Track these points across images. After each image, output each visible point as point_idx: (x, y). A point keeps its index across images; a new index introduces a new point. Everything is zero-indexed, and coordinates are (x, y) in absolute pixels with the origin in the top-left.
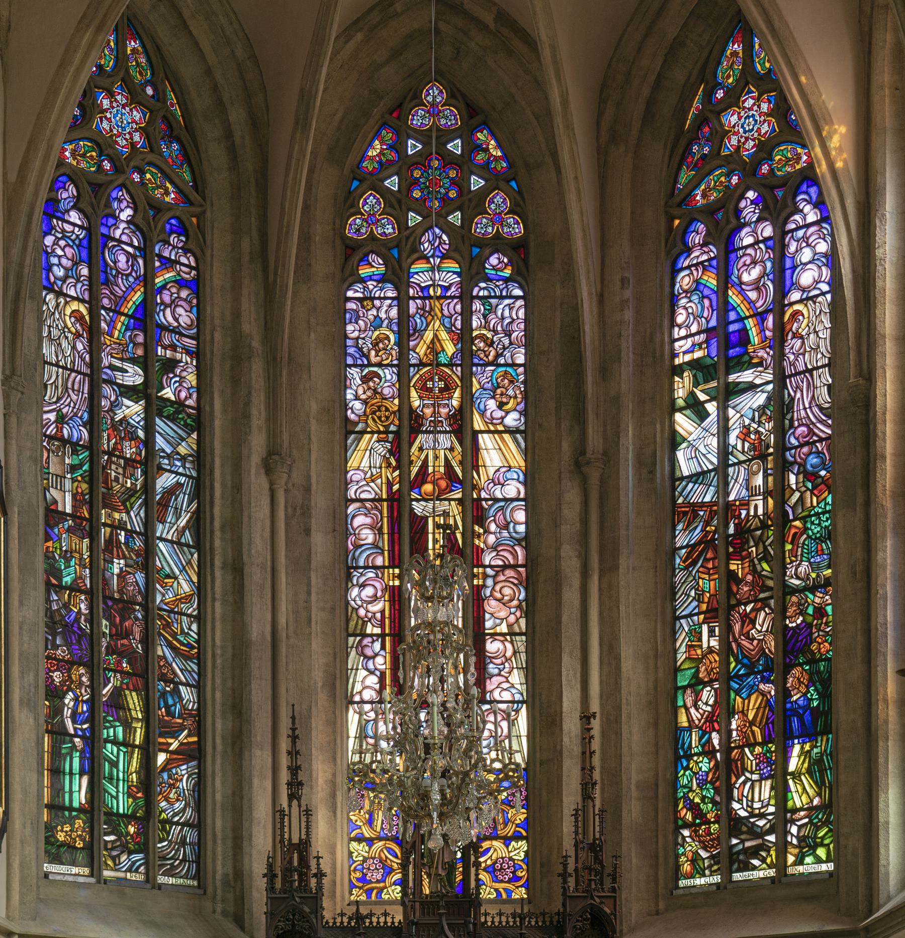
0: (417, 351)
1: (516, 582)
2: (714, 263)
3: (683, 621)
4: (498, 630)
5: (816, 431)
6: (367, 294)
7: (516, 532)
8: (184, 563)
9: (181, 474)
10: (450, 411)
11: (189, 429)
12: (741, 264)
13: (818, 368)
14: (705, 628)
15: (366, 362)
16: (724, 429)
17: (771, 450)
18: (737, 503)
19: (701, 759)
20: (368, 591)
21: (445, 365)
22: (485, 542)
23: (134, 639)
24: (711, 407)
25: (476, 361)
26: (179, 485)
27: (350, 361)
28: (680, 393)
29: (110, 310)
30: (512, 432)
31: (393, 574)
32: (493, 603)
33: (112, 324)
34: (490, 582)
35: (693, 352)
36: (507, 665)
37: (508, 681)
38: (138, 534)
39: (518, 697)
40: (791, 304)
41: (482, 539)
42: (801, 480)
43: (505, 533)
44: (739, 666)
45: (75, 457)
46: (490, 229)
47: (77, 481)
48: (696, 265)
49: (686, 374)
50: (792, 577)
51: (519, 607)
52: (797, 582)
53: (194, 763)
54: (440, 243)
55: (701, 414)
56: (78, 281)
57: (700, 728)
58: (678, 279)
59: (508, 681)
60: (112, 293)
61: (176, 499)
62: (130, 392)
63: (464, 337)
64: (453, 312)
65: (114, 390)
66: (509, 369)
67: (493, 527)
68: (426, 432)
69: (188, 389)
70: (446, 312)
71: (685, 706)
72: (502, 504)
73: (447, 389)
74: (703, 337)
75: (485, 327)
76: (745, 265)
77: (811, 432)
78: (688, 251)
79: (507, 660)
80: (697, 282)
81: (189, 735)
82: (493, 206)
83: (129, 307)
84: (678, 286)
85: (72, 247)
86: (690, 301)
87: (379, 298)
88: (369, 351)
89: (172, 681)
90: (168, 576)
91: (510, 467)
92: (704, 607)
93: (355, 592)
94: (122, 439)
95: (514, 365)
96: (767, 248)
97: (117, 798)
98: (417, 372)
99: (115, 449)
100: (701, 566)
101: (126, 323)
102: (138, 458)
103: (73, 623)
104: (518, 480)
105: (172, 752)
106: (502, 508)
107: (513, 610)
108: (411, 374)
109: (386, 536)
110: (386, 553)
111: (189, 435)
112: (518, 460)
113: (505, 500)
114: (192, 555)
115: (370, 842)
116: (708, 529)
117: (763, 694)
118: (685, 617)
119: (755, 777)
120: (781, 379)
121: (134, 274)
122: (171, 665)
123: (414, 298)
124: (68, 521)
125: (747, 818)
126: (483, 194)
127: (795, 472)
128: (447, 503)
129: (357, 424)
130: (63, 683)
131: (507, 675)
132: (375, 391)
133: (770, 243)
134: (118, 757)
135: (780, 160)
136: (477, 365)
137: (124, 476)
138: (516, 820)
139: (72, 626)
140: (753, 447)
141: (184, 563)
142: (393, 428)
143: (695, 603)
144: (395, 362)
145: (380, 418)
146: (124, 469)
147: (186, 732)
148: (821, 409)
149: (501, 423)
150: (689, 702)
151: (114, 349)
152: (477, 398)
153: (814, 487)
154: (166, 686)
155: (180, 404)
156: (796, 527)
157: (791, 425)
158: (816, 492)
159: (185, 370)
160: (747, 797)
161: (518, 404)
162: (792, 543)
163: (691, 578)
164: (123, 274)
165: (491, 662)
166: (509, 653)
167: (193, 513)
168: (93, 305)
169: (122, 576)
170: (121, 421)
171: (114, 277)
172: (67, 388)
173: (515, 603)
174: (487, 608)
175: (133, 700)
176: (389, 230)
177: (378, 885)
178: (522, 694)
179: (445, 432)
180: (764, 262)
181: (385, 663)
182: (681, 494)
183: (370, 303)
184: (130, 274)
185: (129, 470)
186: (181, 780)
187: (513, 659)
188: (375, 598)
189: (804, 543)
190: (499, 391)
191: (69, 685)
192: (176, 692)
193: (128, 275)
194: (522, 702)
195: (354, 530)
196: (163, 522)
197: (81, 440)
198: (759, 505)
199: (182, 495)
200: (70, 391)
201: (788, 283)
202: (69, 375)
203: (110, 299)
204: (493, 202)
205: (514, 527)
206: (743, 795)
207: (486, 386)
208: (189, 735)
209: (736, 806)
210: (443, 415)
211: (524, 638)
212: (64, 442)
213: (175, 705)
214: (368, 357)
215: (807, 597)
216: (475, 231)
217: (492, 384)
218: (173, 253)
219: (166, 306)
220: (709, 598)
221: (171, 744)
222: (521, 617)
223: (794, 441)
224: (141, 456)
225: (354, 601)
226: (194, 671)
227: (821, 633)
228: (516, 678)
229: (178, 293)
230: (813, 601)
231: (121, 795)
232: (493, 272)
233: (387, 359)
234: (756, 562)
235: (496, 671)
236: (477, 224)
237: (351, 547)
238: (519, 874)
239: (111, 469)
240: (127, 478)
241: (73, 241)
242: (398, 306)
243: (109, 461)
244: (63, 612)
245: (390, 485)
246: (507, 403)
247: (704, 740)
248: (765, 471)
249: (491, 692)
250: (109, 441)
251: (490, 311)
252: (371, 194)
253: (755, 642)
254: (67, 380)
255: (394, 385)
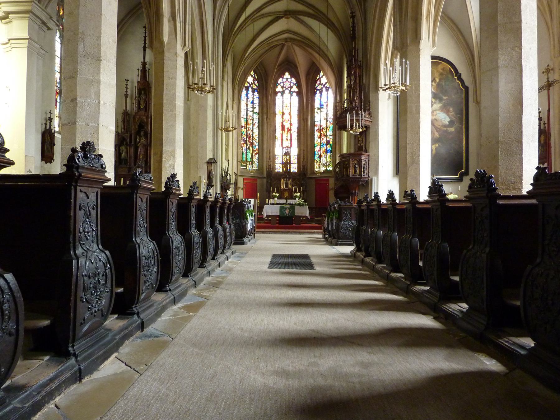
191: (244, 146)
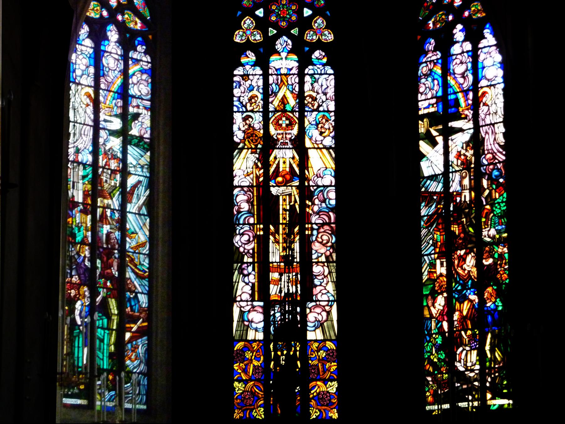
0: (273, 104)
1: (330, 232)
2: (440, 61)
3: (426, 257)
4: (320, 259)
5: (497, 157)
6: (246, 73)
7: (329, 204)
8: (142, 225)
9: (141, 176)
10: (292, 137)
11: (146, 150)
12: (454, 63)
13: (497, 123)
14: (438, 262)
15: (244, 110)
16: (446, 153)
17: (473, 166)
18: (455, 193)
19: (437, 336)
20: (245, 238)
21: (289, 112)
22: (312, 210)
23: (114, 269)
24: (440, 139)
25: (307, 109)
26: (139, 182)
27: (235, 109)
28: (422, 130)
29: (105, 90)
30: (328, 148)
31: (260, 228)
32: (317, 244)
33: (105, 97)
34: (315, 232)
35: (429, 108)
36: (325, 279)
37: (325, 289)
38: (117, 210)
39: (331, 298)
40: (482, 87)
41: (311, 208)
42: (490, 183)
43: (324, 205)
44: (458, 285)
45: (84, 171)
46: (314, 37)
47: (85, 184)
48: (430, 61)
49: (425, 120)
50: (485, 236)
51: (331, 247)
52: (489, 240)
53: (145, 338)
54: (287, 45)
55: (433, 143)
56: (88, 76)
57: (437, 319)
58: (420, 68)
59: (325, 289)
60: (106, 81)
61: (138, 190)
62: (113, 133)
63: (300, 96)
64: (294, 82)
65: (106, 133)
66: (326, 114)
67: (317, 202)
68: (279, 148)
69: (146, 128)
70: (290, 83)
71: (427, 306)
72: (322, 188)
73: (290, 125)
74: (434, 101)
75: (312, 90)
76: (456, 64)
77: (494, 158)
78: (426, 53)
79: (325, 277)
80: (431, 70)
81: (143, 322)
82: (316, 25)
83: (115, 88)
84: (420, 72)
85: (86, 58)
86: (427, 80)
87: (252, 75)
88: (246, 103)
89: (134, 292)
90: (133, 233)
91: (326, 168)
92: (438, 250)
93: (237, 238)
94: (109, 159)
95: (328, 111)
96: (469, 56)
97: (103, 359)
98: (274, 115)
99: (106, 165)
100: (435, 227)
101: (113, 96)
102: (118, 169)
103: (81, 262)
104: (331, 175)
105: (133, 332)
106: (321, 191)
107: (328, 248)
108: (270, 116)
109: (255, 207)
110: (255, 216)
111: (145, 153)
112: (331, 164)
113: (324, 186)
114: (146, 220)
115: (246, 382)
116: (439, 206)
117: (471, 301)
118: (427, 255)
119: (468, 348)
120: (477, 127)
121: (118, 69)
122: (133, 283)
123: (272, 75)
124: (79, 206)
125: (464, 372)
126: (311, 17)
127: (486, 178)
128: (290, 188)
129: (239, 144)
130: (75, 296)
131: (325, 285)
132: (250, 125)
133: (470, 54)
134: (104, 336)
135: (474, 10)
136: (307, 111)
137: (110, 179)
138: (330, 369)
139: (81, 264)
140: (462, 163)
141: (142, 225)
142: (259, 146)
143: (432, 248)
144: (261, 110)
145: (252, 140)
146: (110, 175)
147: (141, 320)
148: (500, 146)
149: (321, 143)
150: (430, 304)
151: (106, 111)
152: (307, 130)
153: (497, 187)
154: (131, 295)
155: (141, 138)
156: (487, 209)
157: (484, 153)
158: (497, 190)
159: (144, 118)
160: (464, 360)
161: (331, 133)
162: (485, 218)
163: (430, 233)
164: (112, 70)
165: (316, 278)
166: (326, 273)
167: (147, 197)
168: (97, 88)
169: (108, 234)
170: (109, 150)
171: (107, 72)
172: (81, 134)
173: (329, 244)
174: (313, 247)
175: (113, 304)
176: (258, 37)
177: (250, 407)
178: (334, 296)
179: (290, 148)
180: (467, 63)
181: (255, 278)
182: (423, 186)
183: (247, 78)
184: (116, 70)
185: (113, 175)
186: (138, 348)
187: (329, 276)
188: (249, 241)
189: (492, 218)
190: (320, 126)
192: (136, 297)
193: (114, 70)
194: (334, 301)
195: (237, 203)
196: (131, 202)
197: (88, 161)
198: (467, 196)
199: (141, 187)
200: (83, 136)
201: (480, 76)
202: (83, 127)
203: (105, 84)
204: (317, 22)
205: (329, 202)
206: (461, 359)
207: (312, 123)
208: (143, 322)
209: (458, 364)
210: (288, 139)
211: (335, 264)
212: (79, 163)
213: (135, 305)
214: (246, 107)
215: (494, 248)
216: (306, 38)
217: (316, 122)
218: (139, 56)
219: (135, 84)
220: (440, 245)
221: (132, 328)
222: (333, 252)
223: (486, 163)
224: (119, 167)
225: (237, 243)
226: (146, 285)
227: (502, 269)
228: (331, 287)
229: (141, 77)
230: (497, 251)
231: (105, 358)
232: (317, 60)
233: (256, 108)
234: (466, 227)
235: (319, 283)
236: (307, 34)
237: (235, 213)
238: (333, 401)
239: (103, 176)
240: (112, 180)
241: (86, 55)
242: (263, 79)
243: (103, 172)
244: (76, 256)
245: (258, 177)
246: (324, 132)
247: (438, 326)
248: (470, 176)
249: (316, 295)
250: (103, 160)
251: (315, 82)
252: (248, 18)
253: (466, 272)
254: (81, 129)
255: (260, 122)
